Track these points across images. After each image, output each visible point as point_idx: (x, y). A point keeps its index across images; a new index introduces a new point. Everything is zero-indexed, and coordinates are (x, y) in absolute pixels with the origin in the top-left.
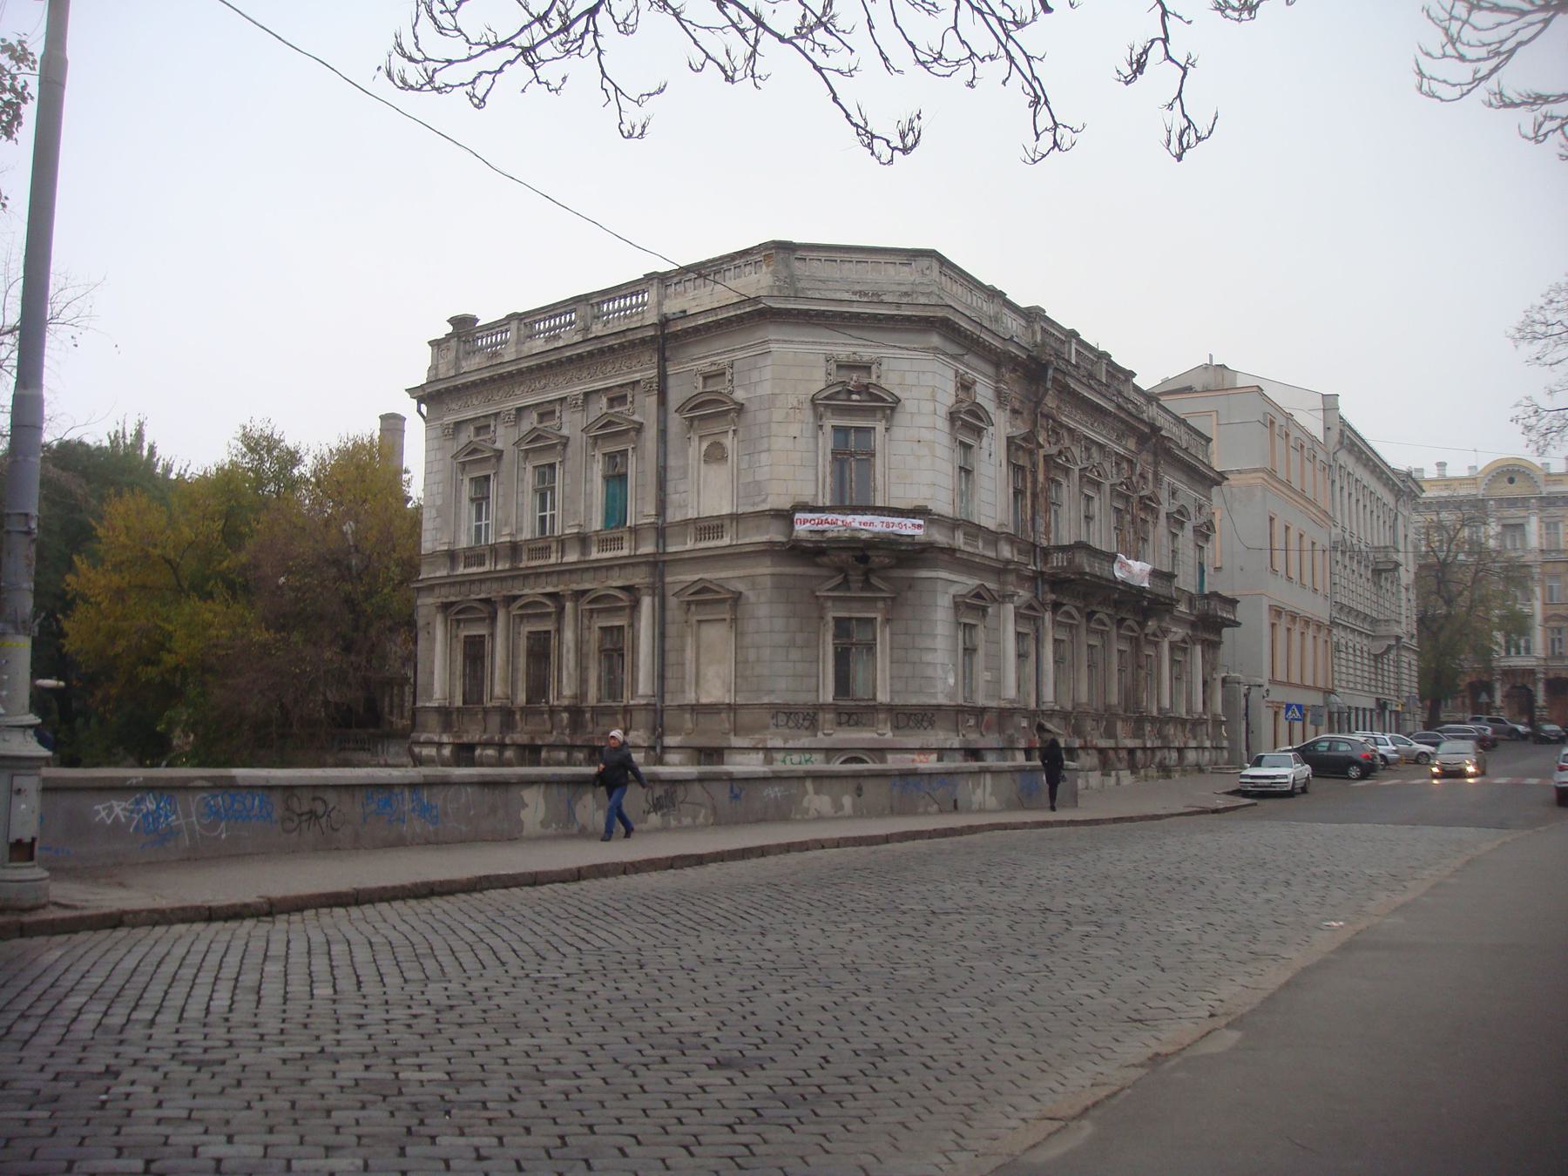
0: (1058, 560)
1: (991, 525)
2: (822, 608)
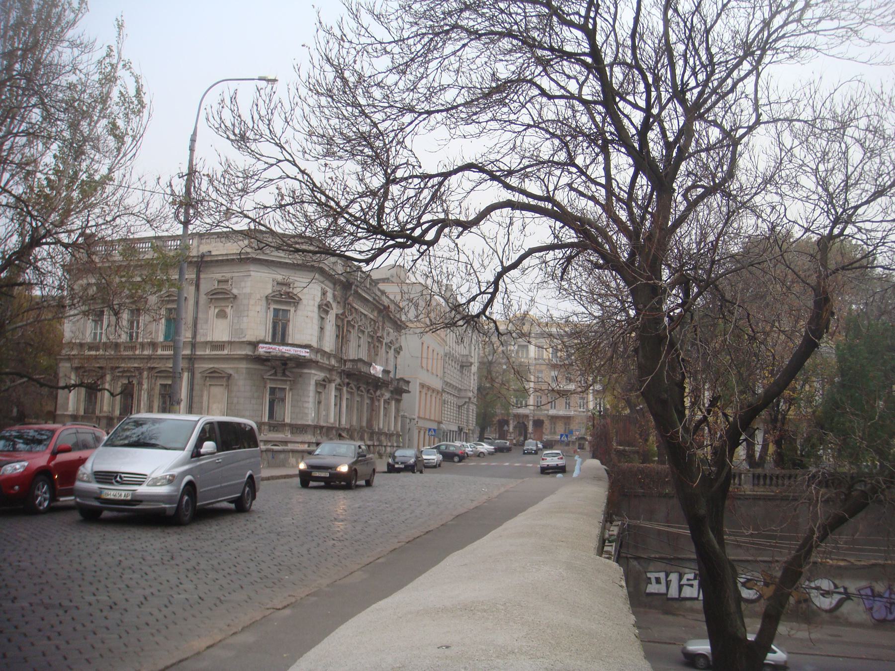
0: (349, 365)
1: (327, 350)
2: (265, 383)
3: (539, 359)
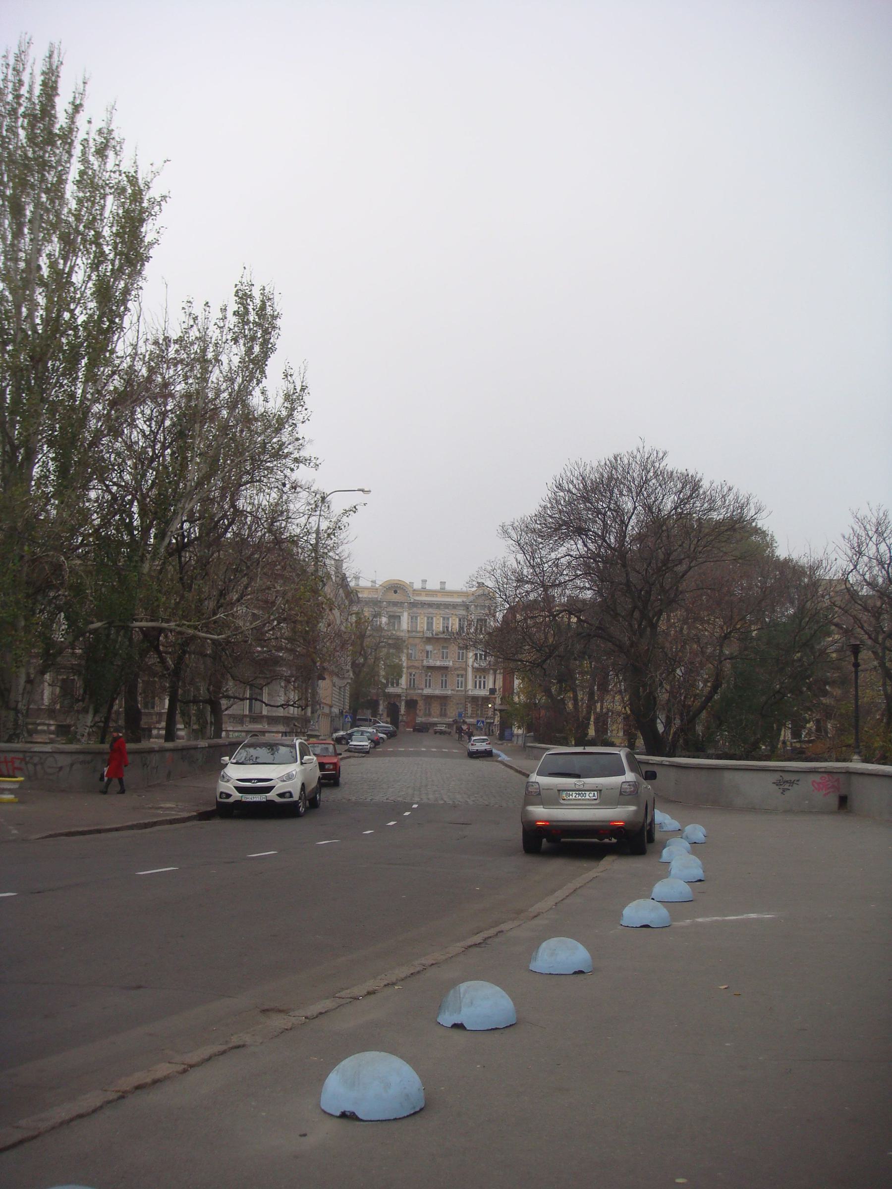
3: (412, 632)
